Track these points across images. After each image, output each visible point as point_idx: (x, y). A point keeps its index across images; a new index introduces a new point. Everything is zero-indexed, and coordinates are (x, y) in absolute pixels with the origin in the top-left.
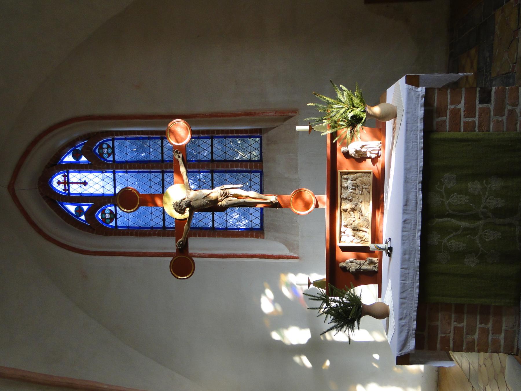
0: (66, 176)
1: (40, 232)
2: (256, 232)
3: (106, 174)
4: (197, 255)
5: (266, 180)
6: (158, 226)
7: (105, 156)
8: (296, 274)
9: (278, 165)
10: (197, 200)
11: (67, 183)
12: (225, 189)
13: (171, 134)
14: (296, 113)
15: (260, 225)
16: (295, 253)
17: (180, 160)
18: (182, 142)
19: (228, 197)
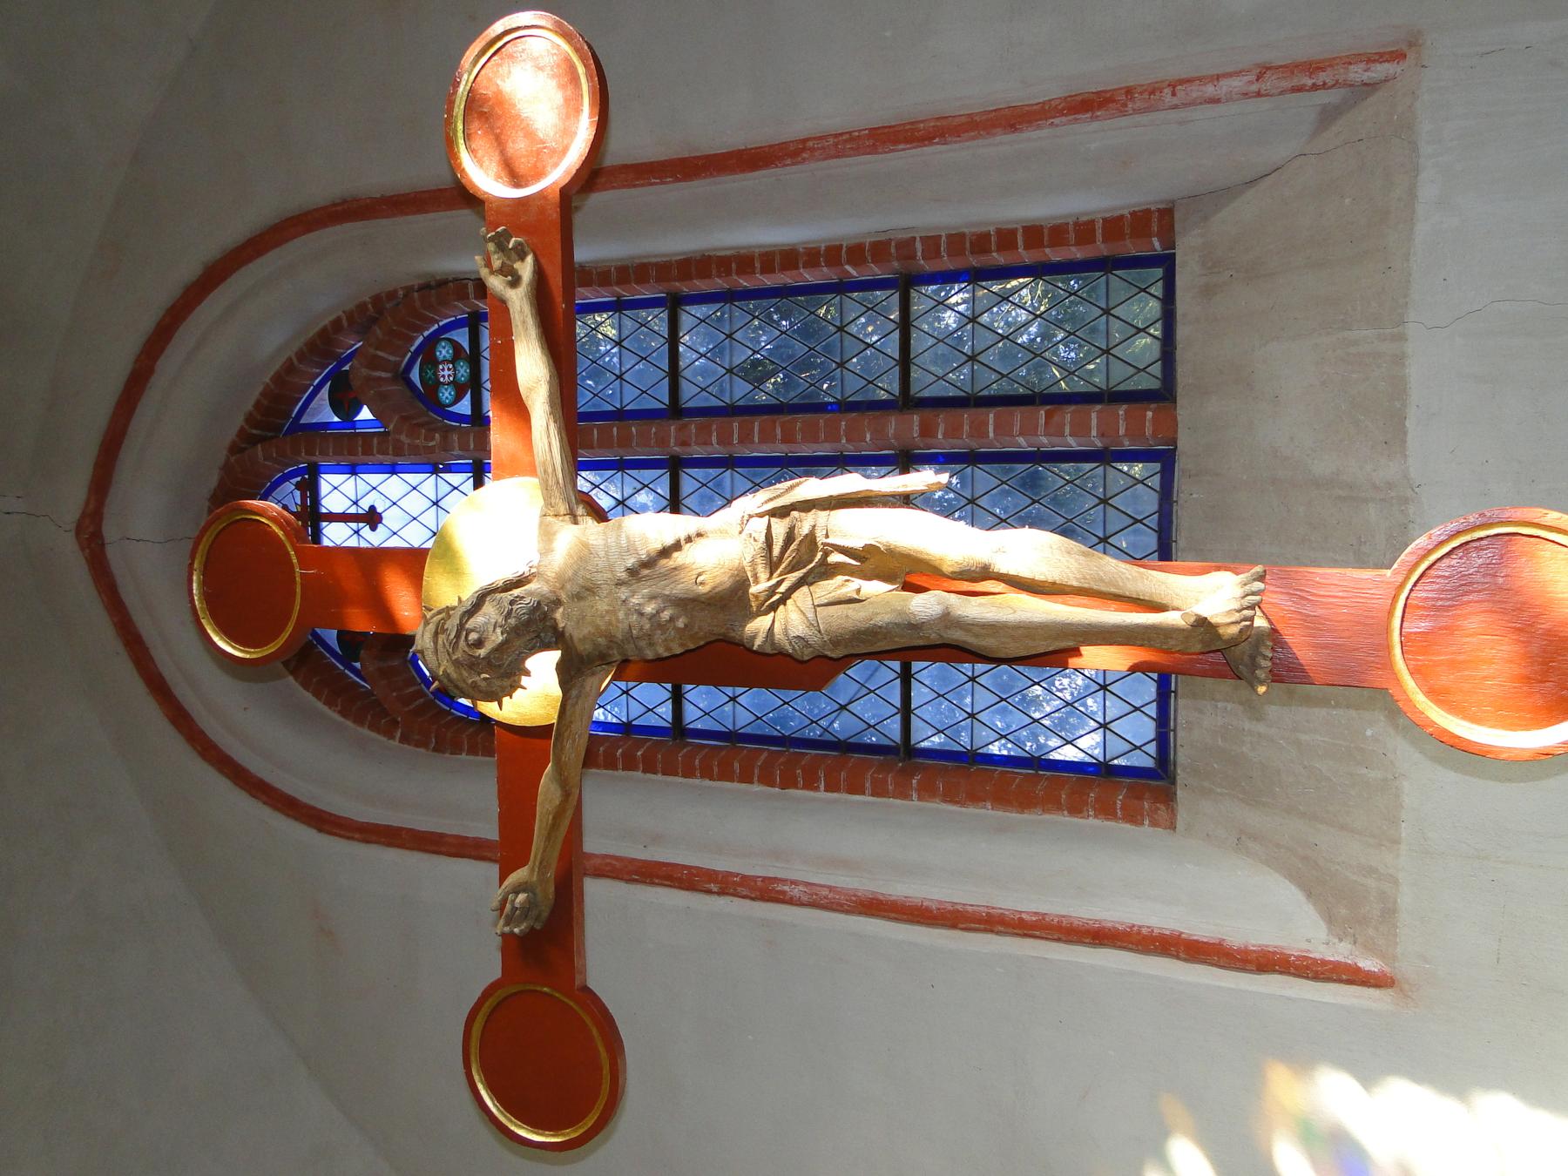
0: (310, 489)
1: (181, 718)
2: (1137, 789)
3: (446, 476)
4: (796, 892)
5: (1187, 492)
6: (651, 720)
7: (446, 395)
8: (1368, 1077)
9: (1263, 395)
10: (587, 590)
11: (313, 516)
12: (807, 506)
13: (475, 125)
14: (1398, 56)
15: (1152, 749)
16: (1370, 948)
17: (518, 301)
18: (539, 174)
19: (827, 571)
